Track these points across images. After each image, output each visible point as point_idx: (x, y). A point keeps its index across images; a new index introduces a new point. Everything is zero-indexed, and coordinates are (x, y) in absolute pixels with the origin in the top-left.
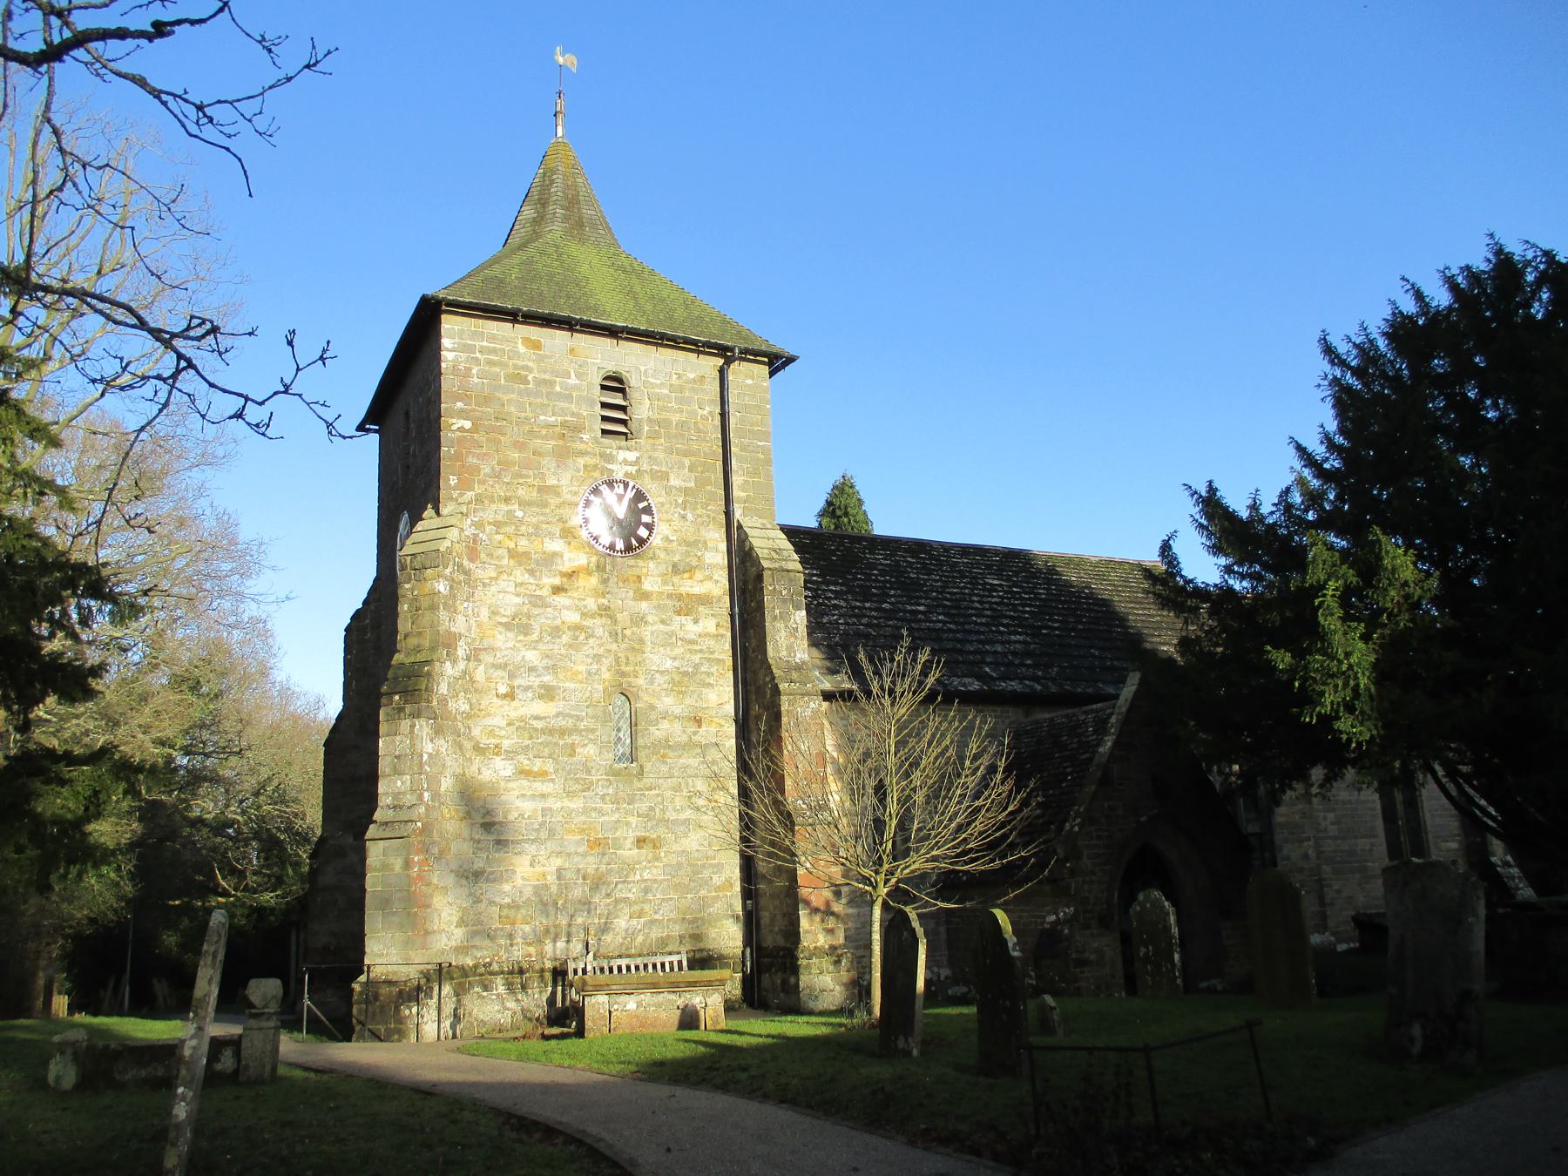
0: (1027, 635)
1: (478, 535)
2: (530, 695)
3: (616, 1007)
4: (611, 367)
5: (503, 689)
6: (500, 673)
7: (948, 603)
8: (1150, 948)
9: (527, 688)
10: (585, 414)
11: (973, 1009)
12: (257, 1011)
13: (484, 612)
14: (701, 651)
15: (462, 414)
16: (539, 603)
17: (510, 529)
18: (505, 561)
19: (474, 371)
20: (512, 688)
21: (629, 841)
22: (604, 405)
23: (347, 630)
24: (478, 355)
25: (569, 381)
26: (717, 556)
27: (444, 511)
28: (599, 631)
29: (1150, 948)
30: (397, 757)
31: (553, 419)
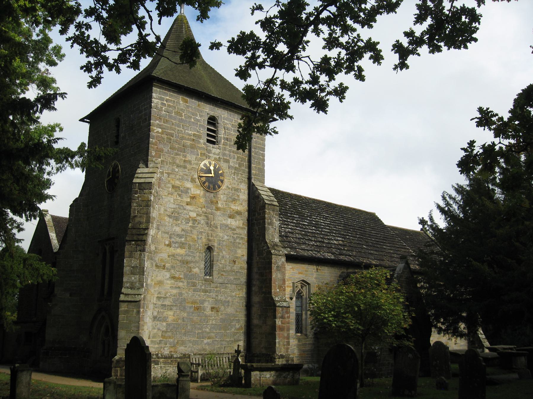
0: (343, 238)
1: (161, 177)
2: (177, 245)
3: (263, 376)
4: (212, 113)
5: (167, 243)
6: (166, 235)
7: (314, 222)
8: (438, 362)
9: (176, 243)
10: (202, 132)
11: (318, 379)
12: (185, 374)
13: (162, 209)
14: (237, 233)
15: (159, 126)
16: (181, 208)
17: (173, 176)
18: (170, 189)
19: (163, 109)
20: (170, 242)
21: (209, 308)
22: (209, 130)
23: (71, 206)
24: (165, 102)
25: (197, 117)
26: (244, 196)
27: (151, 165)
28: (202, 222)
29: (438, 362)
30: (133, 267)
31: (191, 132)
